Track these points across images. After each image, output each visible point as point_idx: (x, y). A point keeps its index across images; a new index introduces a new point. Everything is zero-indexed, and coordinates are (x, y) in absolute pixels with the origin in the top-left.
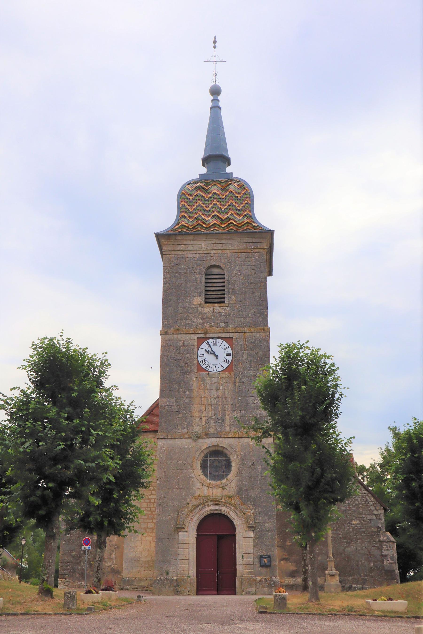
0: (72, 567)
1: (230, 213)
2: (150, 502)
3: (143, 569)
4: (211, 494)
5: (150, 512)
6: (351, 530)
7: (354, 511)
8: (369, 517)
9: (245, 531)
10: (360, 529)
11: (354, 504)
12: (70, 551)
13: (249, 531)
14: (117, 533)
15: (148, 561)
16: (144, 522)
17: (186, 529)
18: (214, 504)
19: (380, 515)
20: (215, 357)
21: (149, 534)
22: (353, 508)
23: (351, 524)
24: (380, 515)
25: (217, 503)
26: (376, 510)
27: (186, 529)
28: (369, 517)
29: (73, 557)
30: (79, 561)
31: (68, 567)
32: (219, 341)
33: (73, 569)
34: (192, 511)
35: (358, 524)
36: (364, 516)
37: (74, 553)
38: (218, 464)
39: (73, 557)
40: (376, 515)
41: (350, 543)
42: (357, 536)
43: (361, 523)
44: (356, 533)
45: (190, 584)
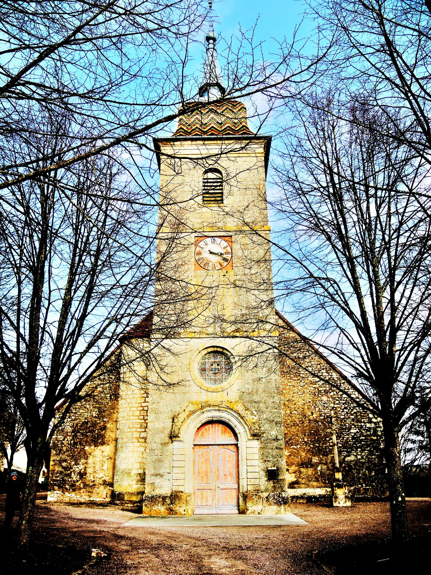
0: (62, 478)
1: (227, 126)
2: (143, 410)
3: (135, 482)
4: (210, 399)
5: (143, 421)
6: (350, 439)
7: (353, 420)
8: (368, 425)
9: (249, 440)
10: (359, 437)
11: (352, 412)
12: (61, 462)
13: (253, 439)
14: (95, 446)
15: (140, 474)
16: (136, 431)
17: (181, 439)
18: (214, 410)
19: (378, 423)
20: (213, 251)
21: (142, 444)
22: (351, 417)
23: (351, 433)
24: (378, 423)
25: (217, 408)
26: (374, 417)
27: (181, 439)
28: (368, 425)
29: (63, 468)
30: (69, 472)
31: (59, 478)
32: (218, 240)
33: (63, 480)
34: (188, 416)
35: (357, 432)
36: (363, 424)
37: (64, 464)
38: (217, 367)
39: (63, 468)
40: (375, 423)
41: (350, 452)
42: (356, 444)
43: (360, 431)
44: (355, 442)
45: (186, 501)
